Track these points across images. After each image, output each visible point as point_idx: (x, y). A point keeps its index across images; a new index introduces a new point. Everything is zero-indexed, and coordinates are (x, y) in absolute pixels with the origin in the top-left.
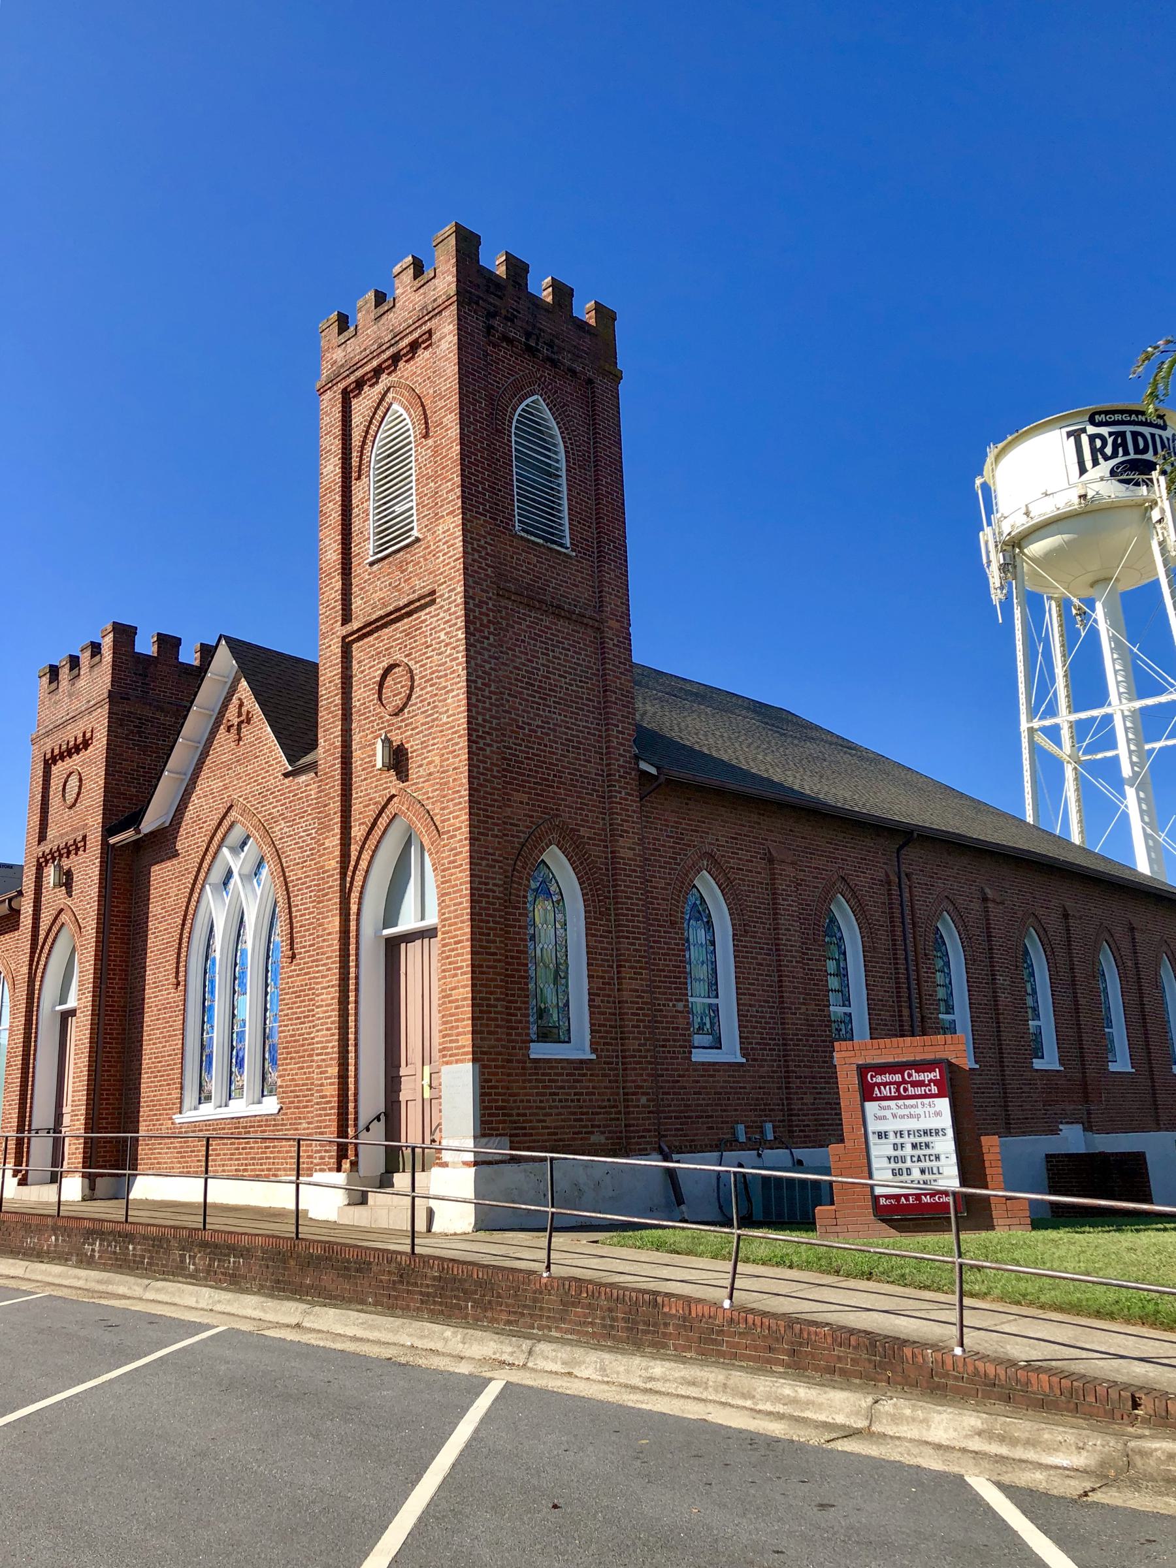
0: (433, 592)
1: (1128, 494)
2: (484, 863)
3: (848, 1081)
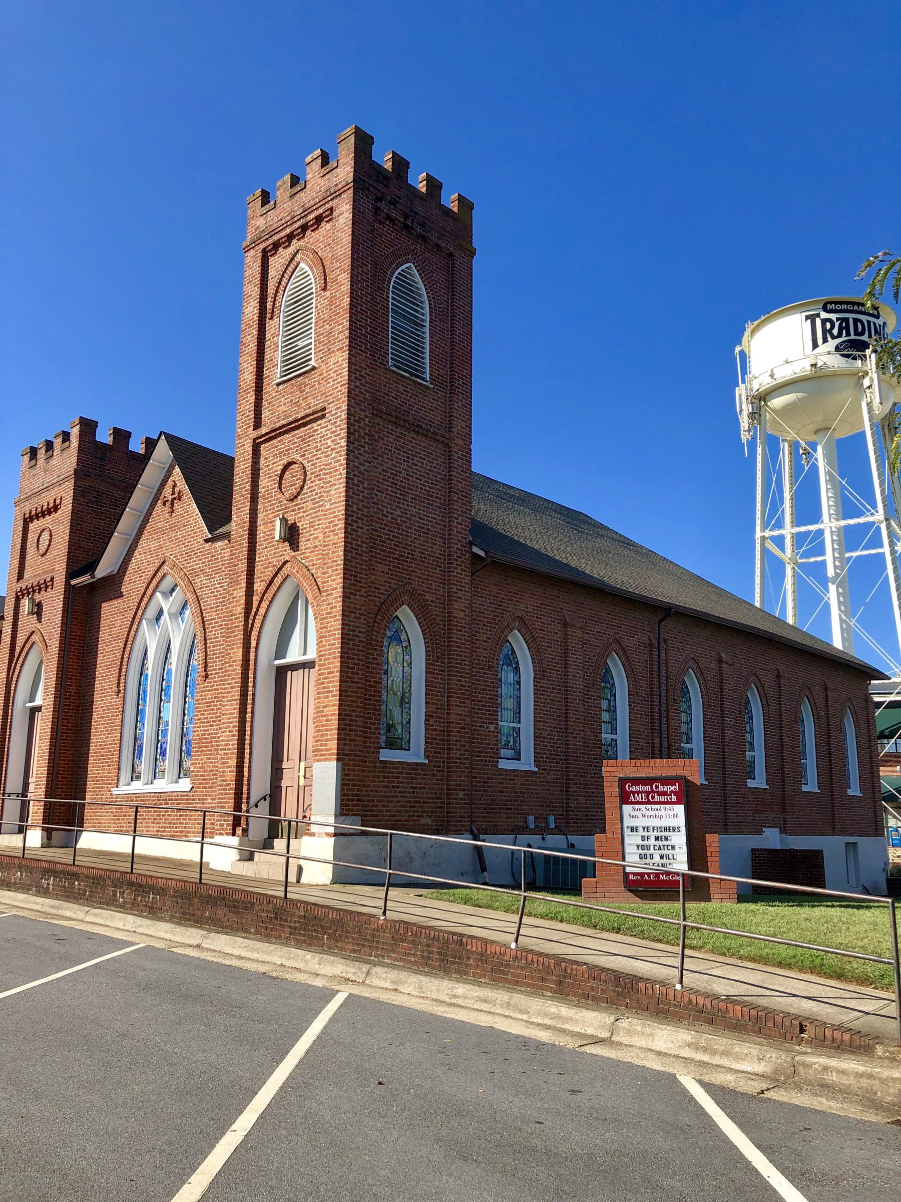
0: (324, 409)
1: (848, 365)
2: (353, 615)
3: (611, 789)
